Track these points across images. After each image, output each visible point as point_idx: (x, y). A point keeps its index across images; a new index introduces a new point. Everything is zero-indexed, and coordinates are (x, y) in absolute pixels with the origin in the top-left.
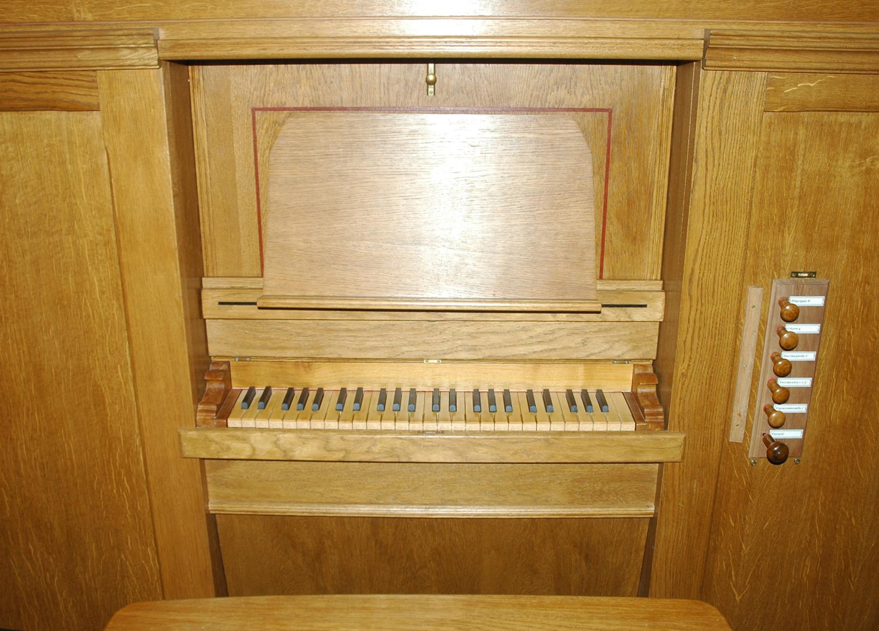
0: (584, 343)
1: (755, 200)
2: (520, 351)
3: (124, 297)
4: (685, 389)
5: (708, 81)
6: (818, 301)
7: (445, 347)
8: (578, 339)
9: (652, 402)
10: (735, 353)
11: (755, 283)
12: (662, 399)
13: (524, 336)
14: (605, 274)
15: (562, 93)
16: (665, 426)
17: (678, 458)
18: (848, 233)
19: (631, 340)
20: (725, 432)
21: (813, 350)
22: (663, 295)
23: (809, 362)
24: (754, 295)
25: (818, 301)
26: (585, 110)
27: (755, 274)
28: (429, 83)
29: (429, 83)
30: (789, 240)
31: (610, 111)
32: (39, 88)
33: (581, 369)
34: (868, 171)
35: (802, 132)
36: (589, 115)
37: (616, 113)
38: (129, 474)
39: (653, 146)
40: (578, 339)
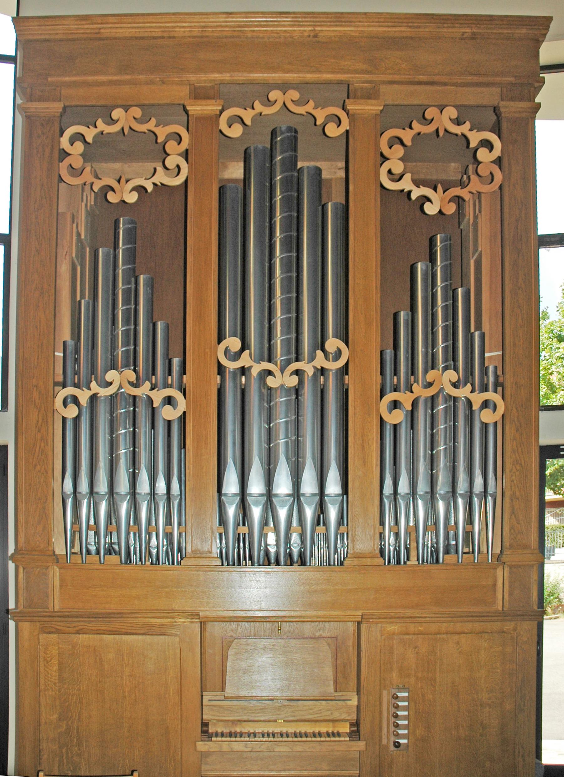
0: (332, 714)
1: (382, 663)
2: (310, 717)
3: (181, 695)
4: (365, 728)
5: (364, 626)
6: (406, 694)
7: (284, 716)
8: (330, 712)
9: (356, 732)
10: (381, 713)
11: (385, 689)
12: (358, 731)
13: (311, 711)
14: (338, 690)
15: (321, 632)
16: (360, 740)
17: (365, 749)
18: (413, 672)
19: (347, 713)
20: (380, 740)
21: (93, 142)
22: (357, 696)
23: (406, 715)
24: (385, 693)
25: (406, 694)
26: (329, 637)
27: (385, 686)
28: (279, 630)
29: (279, 630)
30: (394, 675)
31: (336, 637)
32: (161, 629)
33: (331, 724)
34: (417, 653)
35: (395, 642)
36: (329, 639)
37: (339, 638)
38: (174, 760)
39: (351, 648)
40: (330, 712)
